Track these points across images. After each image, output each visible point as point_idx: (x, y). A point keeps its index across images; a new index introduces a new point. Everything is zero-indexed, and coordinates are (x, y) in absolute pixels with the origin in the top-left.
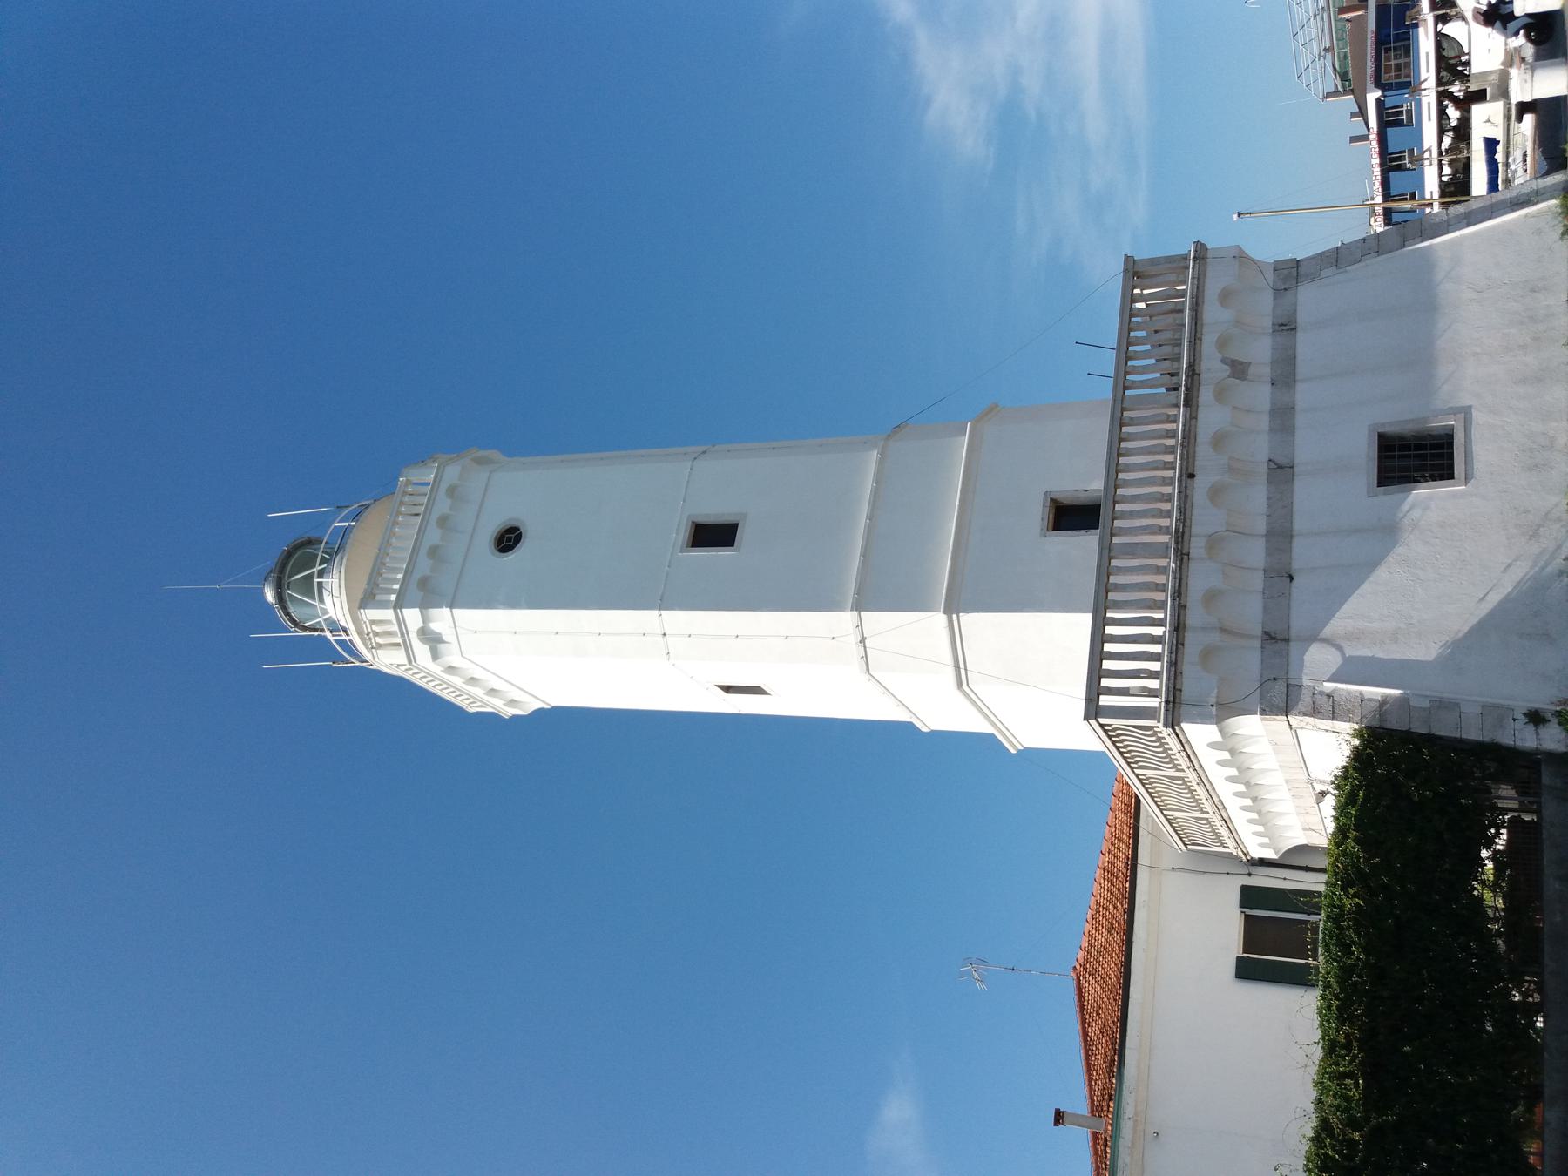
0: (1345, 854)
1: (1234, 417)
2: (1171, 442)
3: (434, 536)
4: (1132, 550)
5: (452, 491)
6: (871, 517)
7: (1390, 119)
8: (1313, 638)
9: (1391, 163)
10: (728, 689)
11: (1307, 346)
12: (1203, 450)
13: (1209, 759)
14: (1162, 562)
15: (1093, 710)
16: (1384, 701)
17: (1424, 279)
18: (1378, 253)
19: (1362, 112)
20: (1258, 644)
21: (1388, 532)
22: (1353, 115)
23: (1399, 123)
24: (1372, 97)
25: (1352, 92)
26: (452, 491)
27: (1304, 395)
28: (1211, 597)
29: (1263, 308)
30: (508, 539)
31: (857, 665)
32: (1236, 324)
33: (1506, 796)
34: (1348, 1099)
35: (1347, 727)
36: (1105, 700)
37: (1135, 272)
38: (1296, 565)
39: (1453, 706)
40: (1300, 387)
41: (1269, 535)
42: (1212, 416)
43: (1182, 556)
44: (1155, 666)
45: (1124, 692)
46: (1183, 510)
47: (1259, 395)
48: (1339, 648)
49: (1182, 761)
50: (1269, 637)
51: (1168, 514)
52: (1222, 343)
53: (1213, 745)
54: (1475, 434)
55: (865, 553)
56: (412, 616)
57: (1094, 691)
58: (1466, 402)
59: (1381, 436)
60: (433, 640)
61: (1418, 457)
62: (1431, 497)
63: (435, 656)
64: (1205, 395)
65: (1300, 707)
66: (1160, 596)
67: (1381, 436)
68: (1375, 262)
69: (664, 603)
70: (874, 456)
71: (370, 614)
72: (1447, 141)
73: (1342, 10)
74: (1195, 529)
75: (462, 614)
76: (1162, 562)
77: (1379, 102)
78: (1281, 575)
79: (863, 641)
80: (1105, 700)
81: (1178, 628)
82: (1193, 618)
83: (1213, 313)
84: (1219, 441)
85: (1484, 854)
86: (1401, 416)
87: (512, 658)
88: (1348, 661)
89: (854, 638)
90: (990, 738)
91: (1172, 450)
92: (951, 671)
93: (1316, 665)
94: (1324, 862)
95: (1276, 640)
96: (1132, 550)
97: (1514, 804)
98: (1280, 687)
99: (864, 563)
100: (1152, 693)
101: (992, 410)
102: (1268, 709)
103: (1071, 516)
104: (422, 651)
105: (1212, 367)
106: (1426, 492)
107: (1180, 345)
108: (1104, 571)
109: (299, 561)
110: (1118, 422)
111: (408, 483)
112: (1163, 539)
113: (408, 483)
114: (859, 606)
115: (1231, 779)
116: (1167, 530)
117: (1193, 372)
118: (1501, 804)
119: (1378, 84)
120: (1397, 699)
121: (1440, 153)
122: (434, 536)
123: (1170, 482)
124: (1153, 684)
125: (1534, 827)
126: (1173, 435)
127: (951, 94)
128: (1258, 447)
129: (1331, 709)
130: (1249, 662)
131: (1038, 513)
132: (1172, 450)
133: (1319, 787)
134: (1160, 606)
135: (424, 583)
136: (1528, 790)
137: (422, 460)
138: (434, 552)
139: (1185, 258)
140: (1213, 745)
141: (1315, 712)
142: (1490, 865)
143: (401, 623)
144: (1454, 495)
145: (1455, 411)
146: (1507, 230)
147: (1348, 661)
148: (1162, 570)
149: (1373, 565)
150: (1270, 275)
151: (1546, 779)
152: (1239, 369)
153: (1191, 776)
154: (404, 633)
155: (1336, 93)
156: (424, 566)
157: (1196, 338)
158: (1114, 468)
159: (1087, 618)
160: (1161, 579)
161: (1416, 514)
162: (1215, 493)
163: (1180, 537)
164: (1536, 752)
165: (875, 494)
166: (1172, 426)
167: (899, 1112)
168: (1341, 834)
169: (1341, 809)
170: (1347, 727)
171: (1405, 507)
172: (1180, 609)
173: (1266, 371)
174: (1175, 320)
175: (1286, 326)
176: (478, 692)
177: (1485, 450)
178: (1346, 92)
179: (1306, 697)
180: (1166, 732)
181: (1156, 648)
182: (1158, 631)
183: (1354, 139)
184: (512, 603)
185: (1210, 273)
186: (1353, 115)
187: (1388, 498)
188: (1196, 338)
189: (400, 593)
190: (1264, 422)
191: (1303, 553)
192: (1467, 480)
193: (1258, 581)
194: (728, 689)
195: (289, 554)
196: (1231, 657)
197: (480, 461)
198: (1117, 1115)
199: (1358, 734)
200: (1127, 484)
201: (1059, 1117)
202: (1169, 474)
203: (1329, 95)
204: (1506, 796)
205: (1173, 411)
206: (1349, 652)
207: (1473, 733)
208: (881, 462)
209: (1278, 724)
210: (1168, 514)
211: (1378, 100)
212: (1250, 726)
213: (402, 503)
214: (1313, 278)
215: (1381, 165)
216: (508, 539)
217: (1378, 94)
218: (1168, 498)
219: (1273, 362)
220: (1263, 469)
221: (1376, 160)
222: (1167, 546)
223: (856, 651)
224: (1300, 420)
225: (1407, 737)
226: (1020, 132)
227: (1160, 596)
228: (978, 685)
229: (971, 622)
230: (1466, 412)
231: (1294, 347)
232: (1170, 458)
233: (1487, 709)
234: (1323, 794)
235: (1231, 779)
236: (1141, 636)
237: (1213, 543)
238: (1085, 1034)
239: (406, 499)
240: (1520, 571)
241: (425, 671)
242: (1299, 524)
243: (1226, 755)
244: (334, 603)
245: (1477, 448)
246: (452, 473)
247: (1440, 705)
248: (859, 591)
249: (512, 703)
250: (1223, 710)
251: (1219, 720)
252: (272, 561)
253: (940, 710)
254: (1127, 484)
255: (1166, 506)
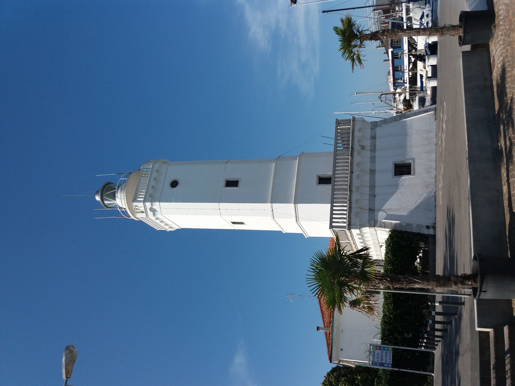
0: (388, 257)
1: (362, 158)
2: (347, 164)
3: (153, 183)
4: (339, 190)
5: (157, 171)
6: (274, 180)
7: (395, 57)
8: (380, 210)
9: (395, 69)
10: (233, 223)
11: (378, 142)
12: (355, 166)
13: (356, 237)
14: (346, 193)
15: (331, 227)
16: (396, 224)
17: (405, 124)
18: (395, 121)
19: (387, 53)
20: (368, 211)
21: (396, 186)
22: (385, 53)
23: (398, 58)
24: (390, 50)
25: (384, 46)
26: (157, 171)
27: (378, 154)
28: (357, 200)
29: (368, 133)
30: (174, 184)
31: (271, 217)
32: (362, 137)
33: (422, 245)
34: (390, 309)
35: (388, 230)
36: (334, 224)
37: (338, 123)
38: (376, 193)
39: (411, 225)
40: (377, 152)
41: (370, 186)
42: (357, 159)
43: (351, 191)
44: (345, 216)
45: (338, 222)
46: (350, 180)
47: (367, 153)
48: (386, 212)
49: (350, 238)
50: (370, 210)
51: (347, 181)
52: (359, 141)
53: (358, 234)
54: (416, 165)
55: (273, 189)
56: (148, 205)
57: (331, 222)
58: (414, 157)
59: (395, 164)
60: (153, 211)
61: (403, 169)
62: (406, 178)
63: (154, 215)
64: (355, 153)
65: (377, 225)
66: (346, 200)
67: (395, 164)
68: (394, 123)
69: (220, 201)
70: (274, 164)
71: (135, 204)
72: (411, 66)
73: (381, 24)
74: (354, 185)
75: (162, 204)
76: (346, 193)
77: (392, 52)
78: (373, 196)
79: (272, 211)
80: (334, 224)
81: (350, 208)
82: (353, 205)
83: (357, 134)
84: (358, 164)
85: (418, 257)
86: (399, 160)
87: (175, 216)
88: (388, 215)
89: (270, 210)
90: (301, 235)
91: (348, 166)
92: (295, 217)
93: (381, 216)
94: (383, 263)
95: (372, 210)
96: (339, 190)
97: (423, 246)
98: (373, 221)
99: (273, 192)
100: (344, 223)
101: (302, 153)
102: (370, 226)
103: (323, 180)
104: (150, 214)
105: (357, 147)
106: (405, 177)
107: (349, 141)
108: (333, 194)
109: (109, 190)
110: (335, 159)
111: (144, 168)
112: (346, 187)
113: (144, 168)
114: (272, 202)
115: (361, 242)
116: (347, 185)
117: (352, 148)
118: (421, 246)
119: (392, 47)
120: (399, 223)
121: (409, 71)
122: (153, 183)
123: (347, 174)
124: (345, 220)
125: (428, 251)
126: (348, 163)
127: (257, 27)
128: (368, 166)
129: (384, 226)
130: (366, 215)
131: (315, 180)
132: (348, 166)
133: (381, 244)
134: (346, 203)
135: (151, 196)
136: (426, 243)
137: (147, 162)
138: (153, 187)
139: (350, 120)
140: (358, 234)
141: (381, 226)
142: (418, 260)
143: (145, 207)
144: (412, 178)
145: (411, 159)
146: (423, 118)
147: (388, 215)
148: (347, 194)
149: (393, 194)
150: (370, 125)
151: (430, 240)
152: (363, 147)
153: (352, 242)
154: (145, 209)
155: (380, 47)
156: (151, 191)
157: (353, 140)
158: (334, 170)
159: (329, 205)
160: (346, 196)
161: (403, 182)
162: (358, 176)
163: (350, 187)
164: (428, 234)
165: (275, 174)
166: (348, 161)
167: (240, 360)
168: (387, 254)
169: (387, 247)
170: (388, 230)
171: (400, 181)
172: (350, 203)
173: (369, 148)
174: (348, 135)
175: (374, 137)
176: (163, 224)
177: (418, 168)
178: (383, 47)
179: (379, 223)
180: (347, 231)
181: (345, 212)
182: (345, 208)
183: (385, 61)
184: (177, 201)
185: (356, 124)
186: (385, 53)
187: (396, 178)
188: (353, 140)
189: (145, 198)
190: (368, 160)
191: (377, 190)
192: (414, 175)
193: (367, 197)
194: (233, 223)
195: (104, 187)
196: (363, 215)
197: (164, 162)
198: (332, 327)
199: (390, 231)
200: (338, 174)
201: (318, 328)
202: (347, 172)
203: (378, 47)
204: (422, 245)
205: (348, 157)
206: (389, 213)
207: (415, 231)
208: (276, 166)
209: (373, 229)
210: (347, 181)
211: (392, 51)
212: (366, 230)
213: (142, 174)
214: (380, 126)
215: (393, 69)
216: (174, 184)
217: (392, 50)
218: (347, 178)
219: (371, 146)
220: (369, 171)
221: (391, 68)
222: (347, 189)
223: (271, 213)
224: (377, 160)
225: (401, 232)
226: (279, 41)
227: (346, 200)
228: (302, 223)
229: (300, 206)
230: (414, 159)
231: (375, 142)
232: (347, 168)
233: (418, 225)
234: (382, 246)
235: (361, 242)
236: (341, 209)
237: (358, 188)
238: (322, 310)
239: (144, 173)
240: (425, 195)
241: (150, 220)
242: (377, 184)
243: (360, 237)
244: (120, 201)
245: (416, 168)
246: (157, 166)
247: (408, 225)
248: (271, 198)
249: (171, 227)
250: (360, 226)
251: (360, 228)
252: (100, 187)
253: (289, 226)
254: (338, 174)
255: (347, 179)
